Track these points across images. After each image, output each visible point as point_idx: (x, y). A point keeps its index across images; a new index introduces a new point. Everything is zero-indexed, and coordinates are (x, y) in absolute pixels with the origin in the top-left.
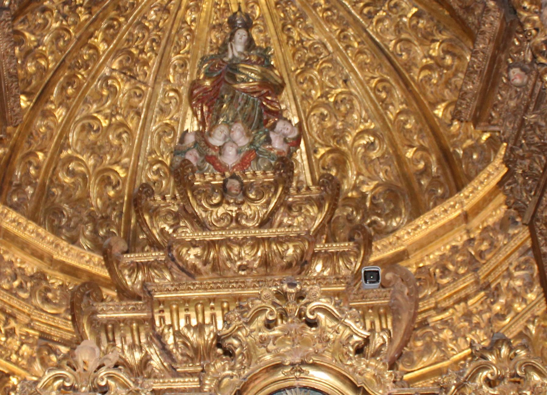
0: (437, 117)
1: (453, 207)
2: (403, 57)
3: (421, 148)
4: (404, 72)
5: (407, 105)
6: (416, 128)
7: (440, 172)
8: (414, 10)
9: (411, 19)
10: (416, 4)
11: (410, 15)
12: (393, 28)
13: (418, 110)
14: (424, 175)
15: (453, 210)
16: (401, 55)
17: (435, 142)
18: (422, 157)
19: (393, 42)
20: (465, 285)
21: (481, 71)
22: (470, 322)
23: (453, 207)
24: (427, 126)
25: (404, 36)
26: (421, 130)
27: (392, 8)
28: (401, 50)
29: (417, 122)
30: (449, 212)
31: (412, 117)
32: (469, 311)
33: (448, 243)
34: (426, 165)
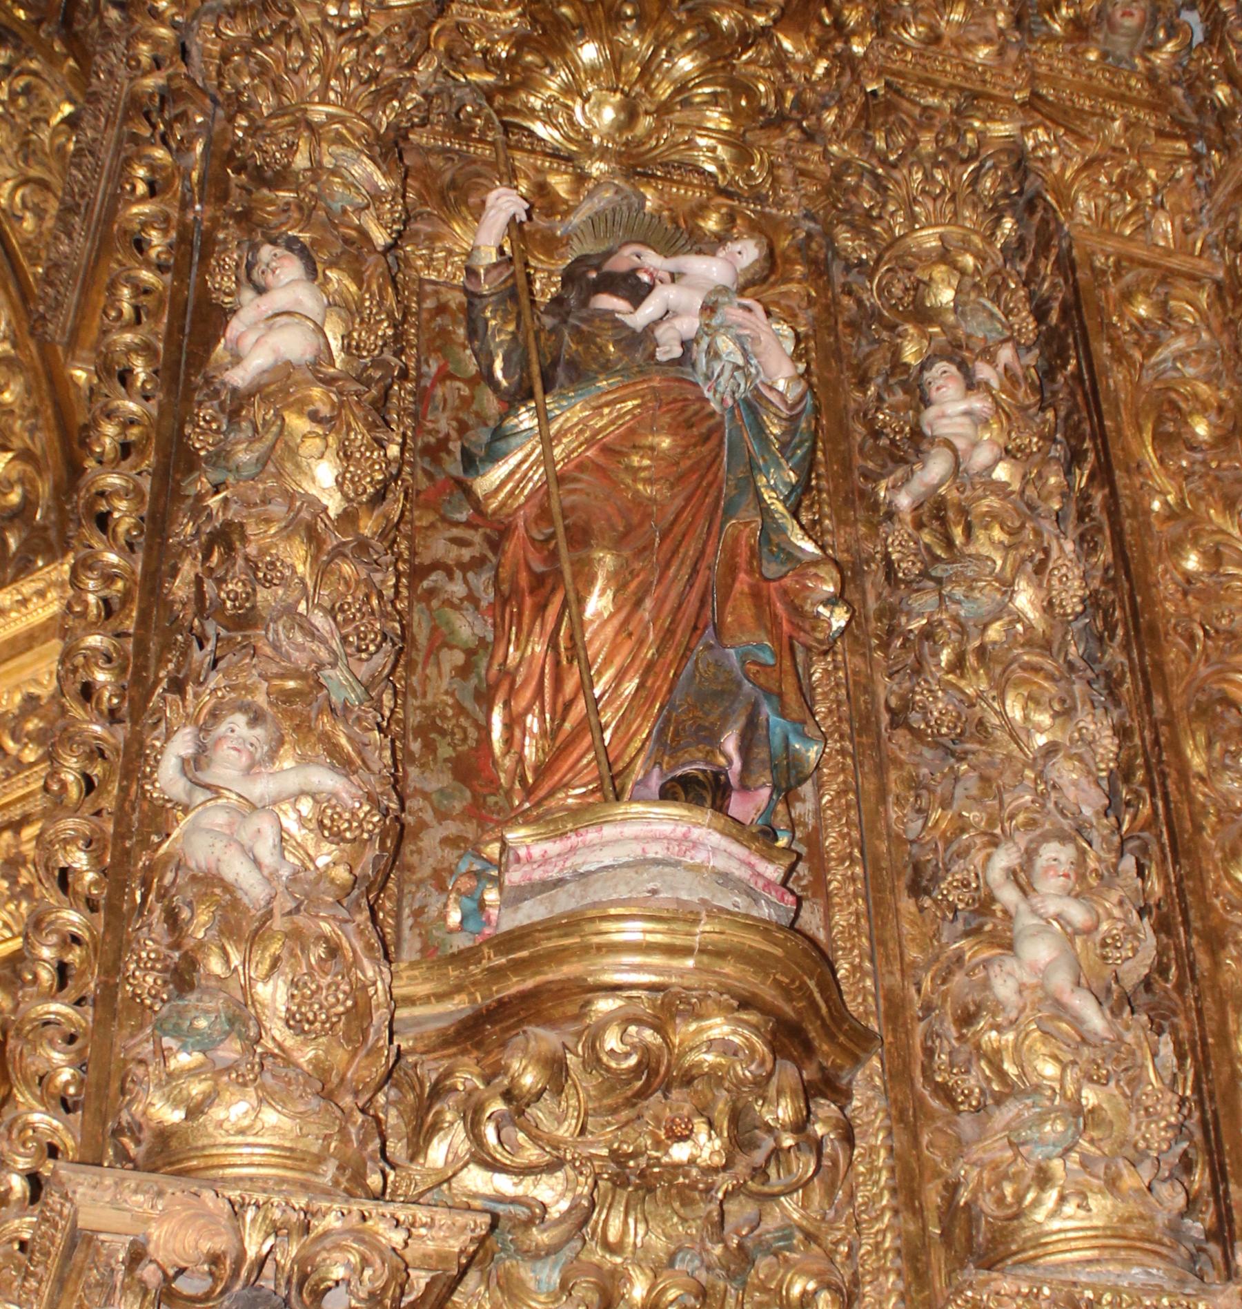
0: (76, 385)
1: (41, 594)
2: (25, 225)
3: (25, 455)
4: (25, 264)
5: (14, 346)
6: (23, 406)
7: (53, 517)
8: (67, 109)
9: (55, 132)
10: (76, 94)
11: (55, 120)
12: (15, 145)
13: (37, 362)
14: (17, 521)
15: (42, 603)
16: (21, 219)
17: (57, 444)
18: (21, 481)
19: (10, 184)
20: (27, 790)
21: (88, 205)
22: (14, 882)
23: (41, 594)
24: (48, 402)
25: (35, 172)
26: (35, 412)
27: (18, 94)
28: (25, 206)
29: (28, 390)
30: (31, 606)
31: (21, 379)
32: (19, 853)
33: (18, 687)
34: (25, 497)
